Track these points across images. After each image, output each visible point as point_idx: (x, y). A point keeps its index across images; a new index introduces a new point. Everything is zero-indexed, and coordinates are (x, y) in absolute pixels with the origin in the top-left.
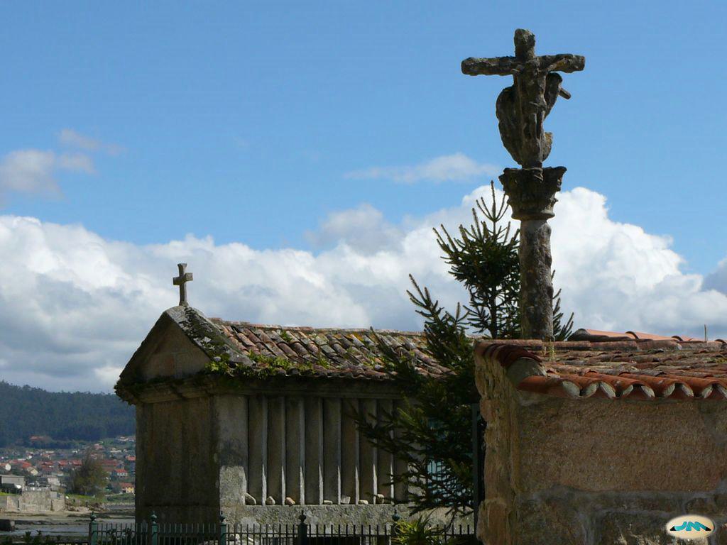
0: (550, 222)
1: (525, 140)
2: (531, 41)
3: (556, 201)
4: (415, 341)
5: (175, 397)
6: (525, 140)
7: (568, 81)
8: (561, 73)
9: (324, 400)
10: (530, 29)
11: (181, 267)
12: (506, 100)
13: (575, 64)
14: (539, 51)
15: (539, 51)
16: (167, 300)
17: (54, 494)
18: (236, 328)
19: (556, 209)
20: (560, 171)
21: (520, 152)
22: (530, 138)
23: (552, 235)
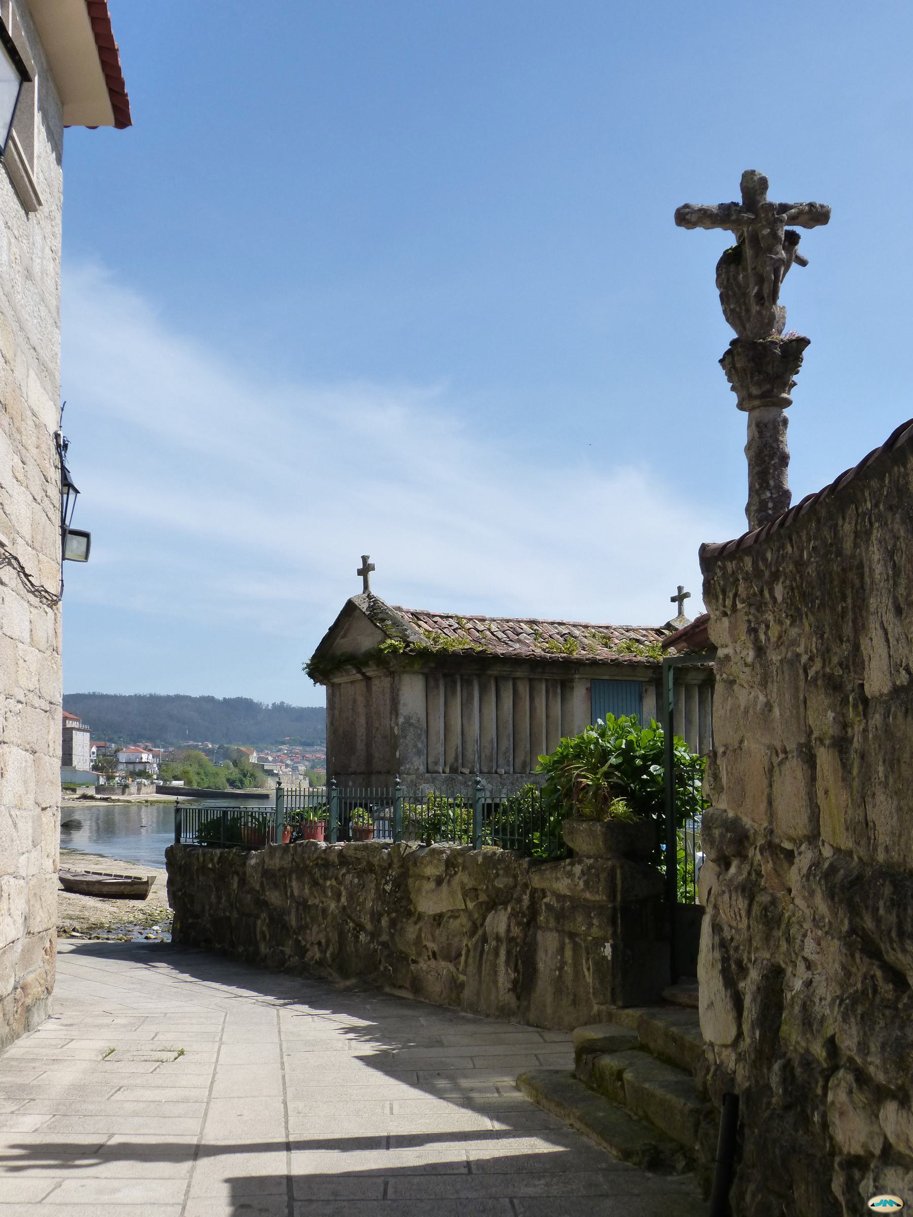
0: (787, 412)
1: (755, 308)
2: (763, 184)
3: (795, 384)
4: (579, 630)
5: (359, 676)
6: (755, 308)
7: (809, 240)
8: (798, 229)
9: (497, 679)
10: (762, 170)
11: (365, 559)
12: (730, 261)
13: (816, 216)
14: (773, 196)
15: (773, 196)
16: (354, 590)
17: (301, 777)
18: (416, 615)
19: (793, 395)
20: (803, 343)
21: (747, 326)
22: (762, 305)
23: (789, 425)
